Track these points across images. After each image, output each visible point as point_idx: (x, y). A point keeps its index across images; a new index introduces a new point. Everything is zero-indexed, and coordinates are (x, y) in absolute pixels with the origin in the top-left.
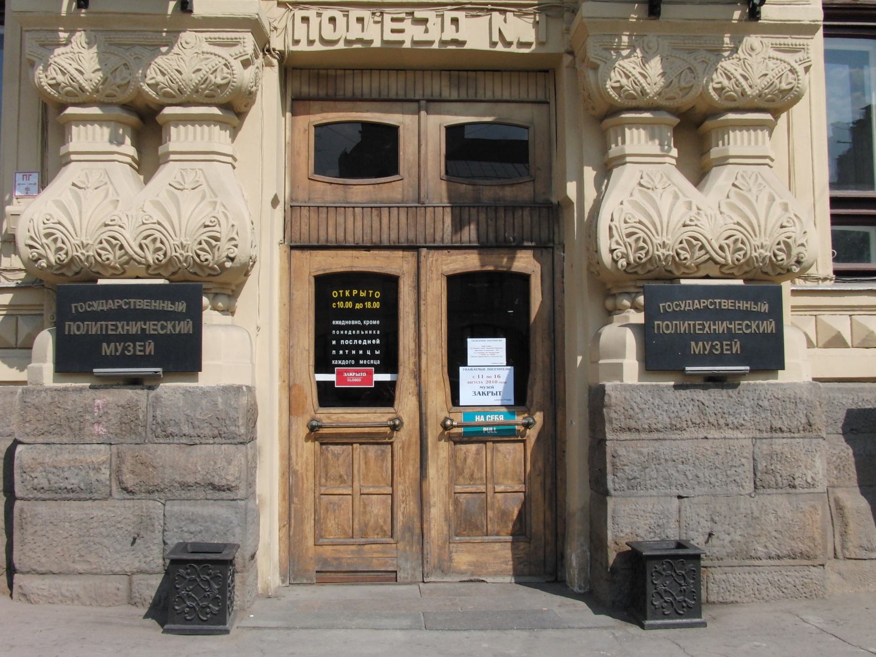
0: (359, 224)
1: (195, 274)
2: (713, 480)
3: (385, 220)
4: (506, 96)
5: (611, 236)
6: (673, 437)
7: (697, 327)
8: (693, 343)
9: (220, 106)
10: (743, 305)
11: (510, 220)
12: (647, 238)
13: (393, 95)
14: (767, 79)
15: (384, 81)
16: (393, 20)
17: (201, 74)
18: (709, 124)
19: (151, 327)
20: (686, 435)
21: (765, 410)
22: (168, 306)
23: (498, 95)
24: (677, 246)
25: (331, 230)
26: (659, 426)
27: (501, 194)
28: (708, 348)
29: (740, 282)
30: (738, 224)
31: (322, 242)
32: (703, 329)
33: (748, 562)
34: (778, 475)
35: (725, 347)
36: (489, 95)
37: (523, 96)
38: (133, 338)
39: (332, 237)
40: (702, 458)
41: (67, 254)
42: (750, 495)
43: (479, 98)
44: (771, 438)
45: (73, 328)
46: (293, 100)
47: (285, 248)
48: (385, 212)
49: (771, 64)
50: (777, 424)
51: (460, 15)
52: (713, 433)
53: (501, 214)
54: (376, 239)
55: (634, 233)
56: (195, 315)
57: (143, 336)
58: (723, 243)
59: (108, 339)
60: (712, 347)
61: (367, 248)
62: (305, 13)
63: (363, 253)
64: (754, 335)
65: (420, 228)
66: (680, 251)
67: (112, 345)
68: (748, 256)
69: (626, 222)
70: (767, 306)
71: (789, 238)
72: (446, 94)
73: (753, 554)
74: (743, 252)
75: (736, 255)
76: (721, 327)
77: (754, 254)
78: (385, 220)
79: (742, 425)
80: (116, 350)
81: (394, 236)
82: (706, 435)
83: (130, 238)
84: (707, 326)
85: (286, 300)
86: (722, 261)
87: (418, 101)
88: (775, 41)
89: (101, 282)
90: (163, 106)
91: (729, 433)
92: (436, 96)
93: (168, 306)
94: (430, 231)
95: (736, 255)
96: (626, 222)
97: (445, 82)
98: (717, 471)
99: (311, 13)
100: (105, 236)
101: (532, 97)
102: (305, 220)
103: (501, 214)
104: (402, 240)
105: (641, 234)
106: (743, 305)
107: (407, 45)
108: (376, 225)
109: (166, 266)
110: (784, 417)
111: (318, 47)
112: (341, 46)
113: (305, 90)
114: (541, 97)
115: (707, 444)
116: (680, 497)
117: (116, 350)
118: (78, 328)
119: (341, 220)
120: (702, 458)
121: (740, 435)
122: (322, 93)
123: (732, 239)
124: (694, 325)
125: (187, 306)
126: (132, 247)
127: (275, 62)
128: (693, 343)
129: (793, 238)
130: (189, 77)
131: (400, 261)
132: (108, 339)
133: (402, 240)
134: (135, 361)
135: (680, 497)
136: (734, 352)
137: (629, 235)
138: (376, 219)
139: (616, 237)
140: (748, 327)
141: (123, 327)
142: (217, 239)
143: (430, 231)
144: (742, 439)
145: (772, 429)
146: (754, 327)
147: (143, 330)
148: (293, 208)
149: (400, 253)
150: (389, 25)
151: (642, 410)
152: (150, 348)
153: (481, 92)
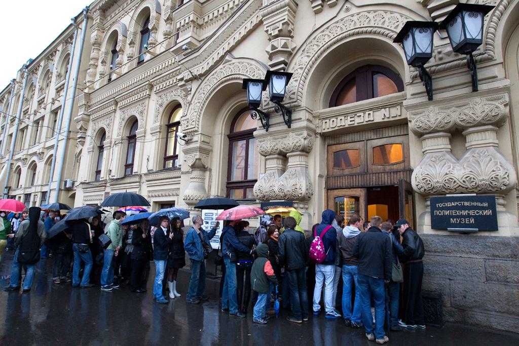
0: (347, 181)
1: (490, 190)
2: (465, 274)
3: (354, 180)
4: (393, 135)
5: (416, 180)
6: (446, 255)
7: (453, 213)
8: (451, 219)
9: (300, 151)
10: (475, 204)
11: (395, 176)
12: (475, 178)
13: (356, 140)
14: (485, 113)
15: (353, 137)
16: (351, 118)
17: (485, 113)
18: (464, 133)
19: (471, 213)
20: (451, 255)
21: (490, 247)
22: (479, 204)
23: (390, 135)
24: (443, 182)
25: (338, 183)
26: (439, 250)
27: (392, 168)
28: (459, 221)
29: (475, 195)
30: (471, 172)
31: (336, 187)
32: (456, 213)
33: (485, 312)
34: (498, 276)
35: (467, 221)
36: (387, 136)
37: (399, 134)
38: (465, 217)
39: (339, 186)
40: (459, 265)
41: (431, 185)
42: (484, 282)
43: (384, 137)
44: (494, 259)
45: (437, 213)
46: (328, 146)
47: (326, 189)
48: (354, 177)
49: (486, 107)
50: (497, 253)
51: (371, 112)
52: (464, 255)
53: (392, 174)
54: (352, 185)
55: (426, 179)
56: (492, 206)
57: (469, 216)
58: (464, 180)
59: (453, 217)
60: (460, 221)
61: (350, 188)
62: (326, 121)
63: (348, 190)
64: (481, 216)
65: (365, 181)
66: (492, 182)
67: (455, 219)
68: (477, 184)
69: (422, 175)
70: (487, 204)
71: (497, 175)
72: (372, 137)
73: (487, 308)
74: (474, 183)
75: (472, 184)
76: (464, 213)
77: (480, 183)
78: (354, 180)
79: (478, 253)
80: (457, 221)
81: (357, 184)
82: (460, 255)
83: (276, 189)
84: (458, 212)
85: (326, 205)
86: (466, 187)
87: (364, 141)
88: (487, 98)
89: (270, 201)
90: (287, 153)
91: (472, 256)
92: (369, 138)
93: (479, 204)
94: (368, 182)
95: (472, 184)
96: (422, 175)
97: (372, 134)
98: (467, 271)
99: (327, 121)
100: (447, 178)
101: (402, 134)
102: (331, 181)
103: (392, 174)
104: (360, 185)
105: (428, 179)
106: (475, 204)
107: (356, 124)
108: (352, 181)
109: (476, 188)
110: (499, 251)
111: (330, 130)
112: (337, 128)
113: (331, 142)
114: (405, 133)
115: (462, 260)
116: (450, 279)
117: (457, 221)
118: (440, 213)
119: (380, 176)
120: (459, 265)
121: (477, 257)
122: (335, 143)
123: (425, 180)
124: (452, 212)
125: (488, 204)
126: (277, 192)
127: (319, 136)
128: (451, 219)
129: (499, 176)
130: (291, 145)
131: (359, 192)
132: (453, 217)
133: (360, 185)
134: (465, 225)
135: (450, 279)
136: (471, 222)
137: (423, 179)
138: (352, 179)
139: (418, 180)
140: (477, 213)
141: (459, 213)
142: (297, 189)
143: (368, 182)
144: (479, 259)
145: (493, 256)
146: (481, 212)
147: (468, 214)
148: (328, 177)
149: (359, 189)
150: (349, 119)
151: (431, 244)
152: (472, 221)
153: (369, 136)
